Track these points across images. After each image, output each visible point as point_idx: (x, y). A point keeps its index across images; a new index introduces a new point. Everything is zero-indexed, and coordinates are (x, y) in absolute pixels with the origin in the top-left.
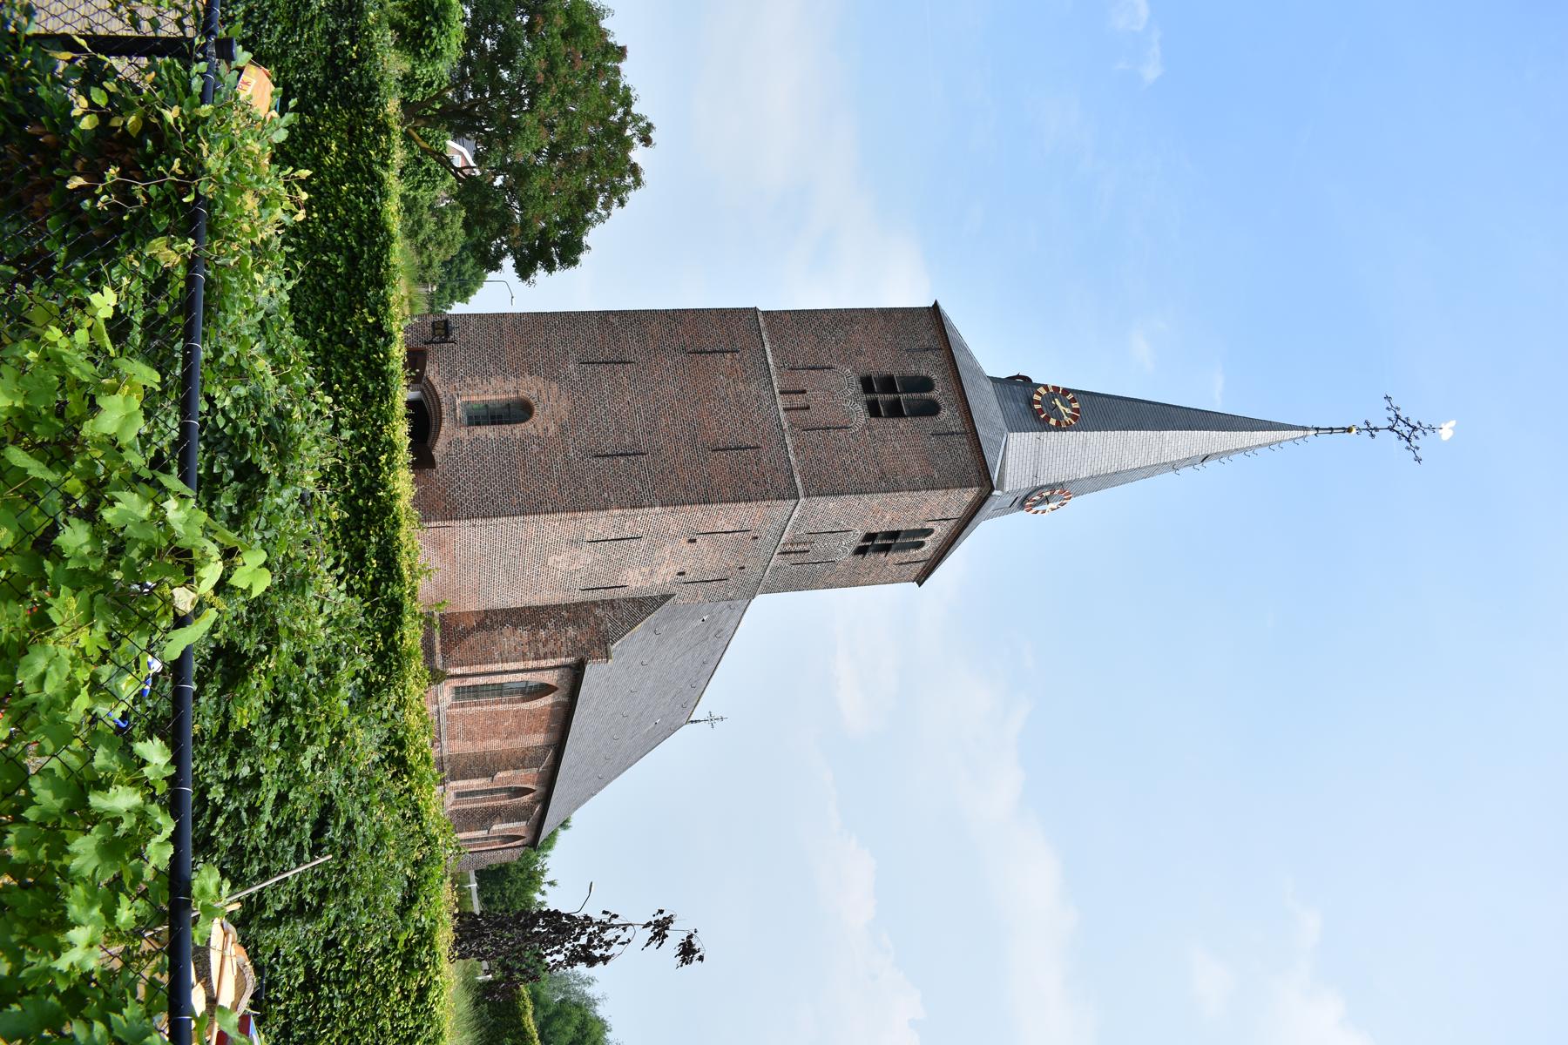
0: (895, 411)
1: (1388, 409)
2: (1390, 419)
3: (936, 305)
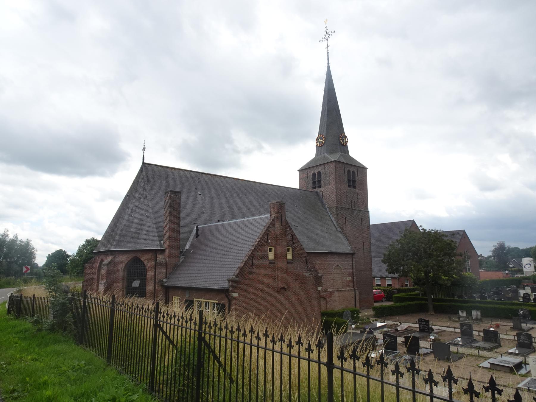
0: (320, 181)
1: (323, 41)
2: (325, 41)
3: (298, 171)
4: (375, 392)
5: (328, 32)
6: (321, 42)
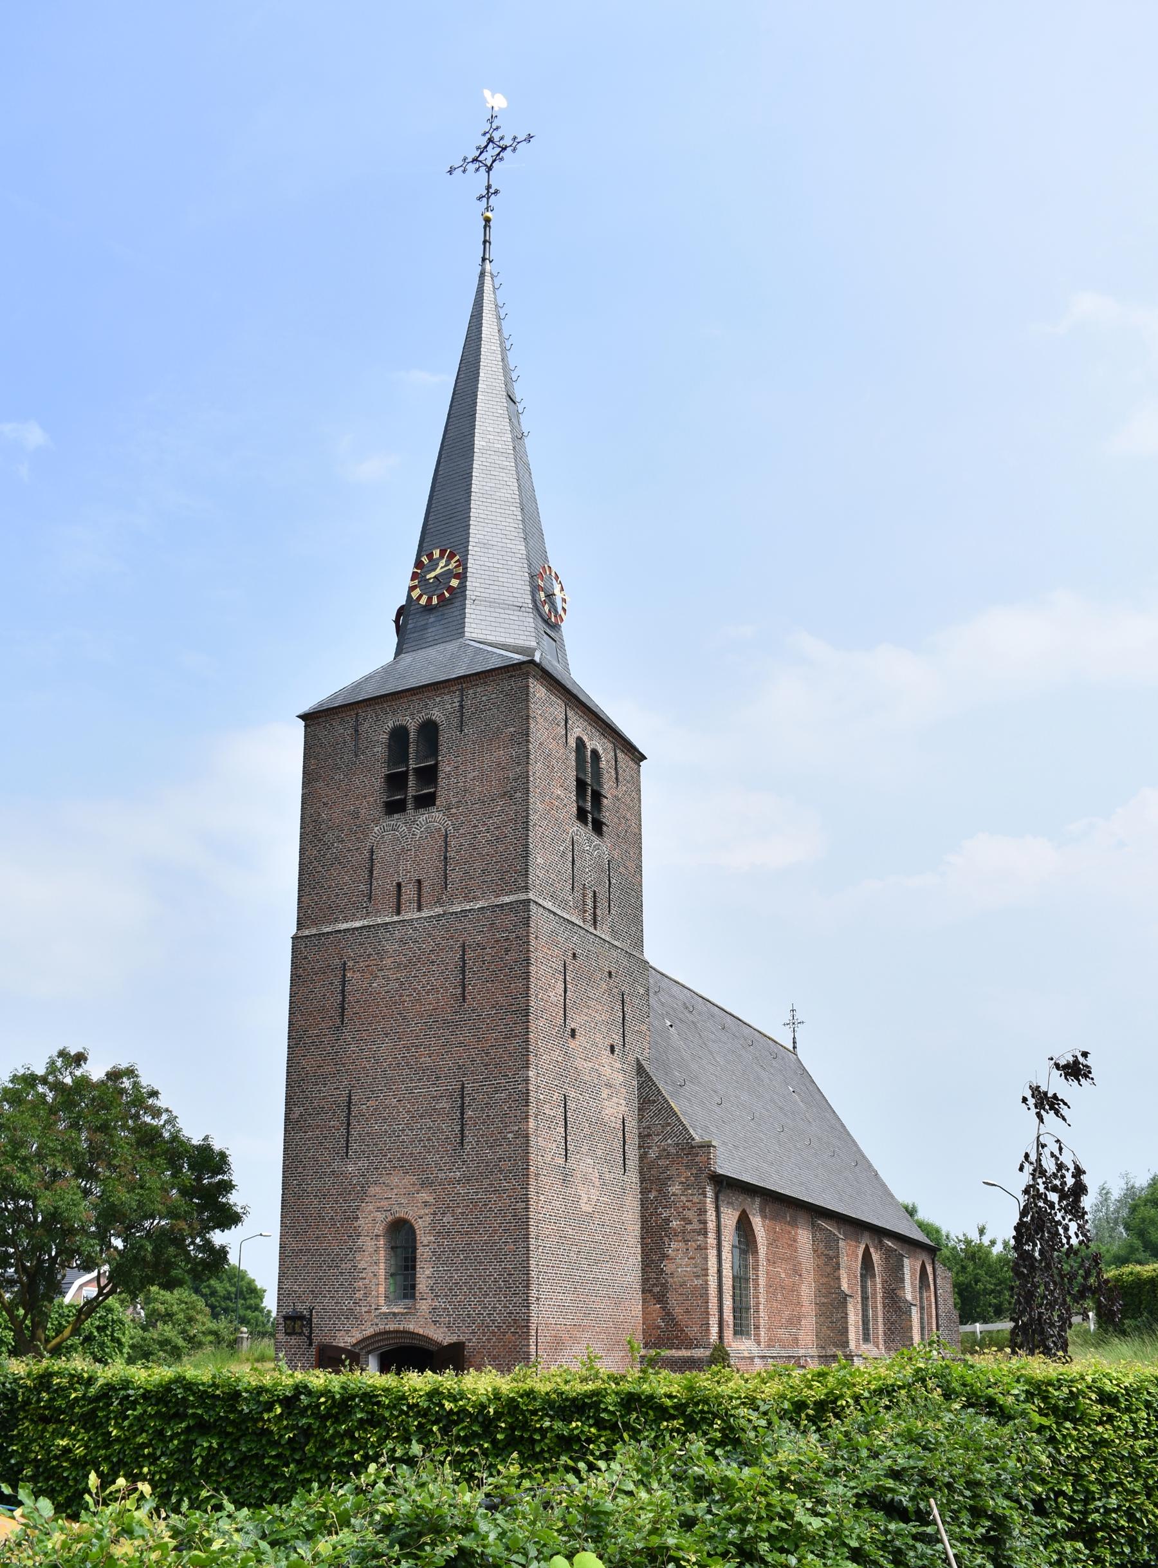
0: (429, 775)
1: (464, 171)
2: (477, 170)
4: (503, 1502)
5: (496, 136)
6: (455, 173)
